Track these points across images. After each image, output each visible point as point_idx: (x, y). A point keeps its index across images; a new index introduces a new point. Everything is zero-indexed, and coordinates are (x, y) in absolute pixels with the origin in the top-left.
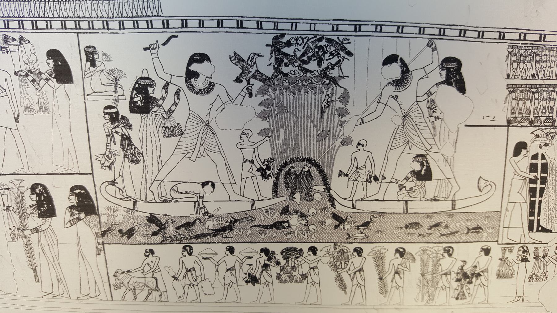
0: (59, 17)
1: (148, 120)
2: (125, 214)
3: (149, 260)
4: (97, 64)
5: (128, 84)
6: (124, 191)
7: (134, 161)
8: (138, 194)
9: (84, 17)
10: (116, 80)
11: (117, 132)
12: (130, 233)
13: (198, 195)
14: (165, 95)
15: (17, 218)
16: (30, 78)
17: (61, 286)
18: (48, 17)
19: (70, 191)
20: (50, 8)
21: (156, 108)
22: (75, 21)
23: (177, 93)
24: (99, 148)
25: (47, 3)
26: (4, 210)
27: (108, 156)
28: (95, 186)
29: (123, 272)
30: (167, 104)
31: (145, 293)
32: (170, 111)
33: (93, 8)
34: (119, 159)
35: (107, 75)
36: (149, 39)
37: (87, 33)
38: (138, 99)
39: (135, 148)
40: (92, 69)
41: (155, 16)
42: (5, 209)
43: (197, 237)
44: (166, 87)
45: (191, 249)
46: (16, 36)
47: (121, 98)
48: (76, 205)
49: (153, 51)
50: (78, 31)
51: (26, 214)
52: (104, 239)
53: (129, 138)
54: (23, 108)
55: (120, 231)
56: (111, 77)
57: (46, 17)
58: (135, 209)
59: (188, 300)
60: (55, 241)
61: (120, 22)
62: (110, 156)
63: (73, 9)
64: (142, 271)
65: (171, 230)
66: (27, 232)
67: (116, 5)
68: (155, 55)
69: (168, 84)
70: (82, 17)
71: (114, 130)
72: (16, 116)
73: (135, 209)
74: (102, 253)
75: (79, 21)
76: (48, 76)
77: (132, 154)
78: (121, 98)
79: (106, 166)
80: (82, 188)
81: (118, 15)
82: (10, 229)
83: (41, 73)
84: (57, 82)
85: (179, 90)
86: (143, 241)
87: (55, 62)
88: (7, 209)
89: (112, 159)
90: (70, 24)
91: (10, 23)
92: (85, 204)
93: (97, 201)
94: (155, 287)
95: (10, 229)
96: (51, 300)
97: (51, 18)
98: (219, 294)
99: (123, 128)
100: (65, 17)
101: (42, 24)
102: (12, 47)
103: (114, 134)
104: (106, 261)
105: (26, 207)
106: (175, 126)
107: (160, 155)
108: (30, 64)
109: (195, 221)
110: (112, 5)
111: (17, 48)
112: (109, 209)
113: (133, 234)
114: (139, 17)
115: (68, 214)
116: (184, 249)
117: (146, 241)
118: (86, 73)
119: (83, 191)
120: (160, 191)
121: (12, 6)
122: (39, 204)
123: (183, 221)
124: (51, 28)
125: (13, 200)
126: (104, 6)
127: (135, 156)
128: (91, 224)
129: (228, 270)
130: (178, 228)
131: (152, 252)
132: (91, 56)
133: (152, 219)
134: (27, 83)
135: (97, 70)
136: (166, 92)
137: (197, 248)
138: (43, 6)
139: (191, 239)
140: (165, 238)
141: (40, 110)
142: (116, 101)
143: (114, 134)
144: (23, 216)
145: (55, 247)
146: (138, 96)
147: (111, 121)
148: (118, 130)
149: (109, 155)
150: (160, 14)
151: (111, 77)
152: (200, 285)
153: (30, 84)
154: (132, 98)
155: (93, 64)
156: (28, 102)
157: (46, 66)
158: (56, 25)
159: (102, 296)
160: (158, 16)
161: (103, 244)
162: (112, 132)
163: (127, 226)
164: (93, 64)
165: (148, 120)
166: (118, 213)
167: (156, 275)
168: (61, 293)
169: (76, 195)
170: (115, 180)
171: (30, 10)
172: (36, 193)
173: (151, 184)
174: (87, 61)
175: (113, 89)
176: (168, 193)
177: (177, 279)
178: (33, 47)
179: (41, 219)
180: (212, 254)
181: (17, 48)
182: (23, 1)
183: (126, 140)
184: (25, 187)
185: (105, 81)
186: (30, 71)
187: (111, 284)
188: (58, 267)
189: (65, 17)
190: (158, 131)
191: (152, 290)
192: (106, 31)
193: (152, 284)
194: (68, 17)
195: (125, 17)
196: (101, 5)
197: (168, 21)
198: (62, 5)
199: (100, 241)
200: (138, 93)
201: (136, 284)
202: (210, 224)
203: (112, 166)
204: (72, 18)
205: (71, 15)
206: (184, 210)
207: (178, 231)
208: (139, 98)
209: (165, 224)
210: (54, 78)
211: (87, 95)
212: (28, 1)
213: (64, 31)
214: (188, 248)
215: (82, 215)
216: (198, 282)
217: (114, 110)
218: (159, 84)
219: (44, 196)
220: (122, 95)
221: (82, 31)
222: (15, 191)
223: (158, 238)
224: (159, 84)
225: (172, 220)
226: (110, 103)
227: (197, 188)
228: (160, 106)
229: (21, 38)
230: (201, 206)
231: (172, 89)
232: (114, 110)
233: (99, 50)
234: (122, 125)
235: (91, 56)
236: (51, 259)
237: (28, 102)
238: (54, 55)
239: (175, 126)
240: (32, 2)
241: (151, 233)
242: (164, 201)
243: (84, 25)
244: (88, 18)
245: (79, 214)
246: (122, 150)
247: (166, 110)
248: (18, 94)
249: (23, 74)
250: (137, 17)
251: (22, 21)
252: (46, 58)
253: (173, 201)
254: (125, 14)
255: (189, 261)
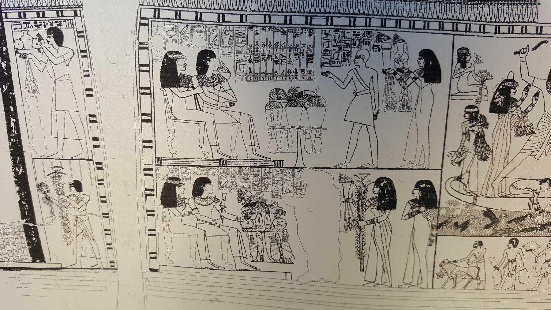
0: (438, 19)
1: (504, 120)
2: (463, 208)
3: (476, 252)
4: (468, 65)
5: (492, 85)
6: (468, 186)
7: (483, 158)
8: (480, 189)
9: (463, 20)
10: (483, 81)
11: (473, 131)
12: (465, 226)
13: (534, 192)
14: (524, 96)
15: (354, 209)
16: (398, 77)
17: (385, 275)
18: (427, 18)
19: (416, 186)
20: (430, 9)
21: (514, 108)
22: (453, 23)
23: (536, 95)
24: (453, 145)
25: (428, 4)
26: (343, 202)
27: (460, 153)
28: (441, 182)
29: (450, 262)
30: (524, 106)
31: (465, 282)
32: (526, 112)
33: (473, 12)
34: (470, 156)
35: (475, 76)
36: (520, 43)
37: (463, 35)
38: (500, 100)
39: (487, 146)
40: (462, 70)
41: (531, 22)
42: (344, 200)
43: (525, 231)
44: (527, 89)
45: (517, 241)
46: (391, 35)
47: (484, 98)
48: (418, 198)
49: (522, 55)
50: (455, 33)
51: (365, 206)
52: (439, 232)
53: (483, 137)
54: (384, 105)
55: (456, 224)
56: (478, 79)
57: (425, 18)
58: (474, 204)
59: (503, 288)
60: (389, 233)
61: (496, 26)
62: (462, 152)
63: (453, 11)
64: (467, 261)
65: (503, 224)
66: (362, 224)
67: (496, 10)
68: (524, 59)
69: (529, 86)
70: (461, 20)
71: (471, 129)
72: (375, 113)
73: (474, 204)
74: (434, 244)
75: (457, 23)
76: (417, 75)
77: (483, 152)
78: (484, 98)
79: (456, 163)
80: (428, 182)
81: (378, 13)
82: (345, 220)
83: (410, 72)
84: (425, 81)
85: (539, 92)
86: (475, 233)
87: (427, 62)
88: (347, 201)
89: (464, 155)
90: (448, 26)
91: (387, 22)
92: (427, 197)
93: (440, 195)
94: (475, 276)
95: (345, 220)
96: (371, 288)
97: (429, 18)
98: (533, 282)
99: (480, 127)
100: (444, 19)
101: (419, 24)
102: (385, 46)
103: (471, 133)
104: (436, 251)
105: (367, 199)
106: (528, 126)
107: (508, 154)
108: (400, 63)
109: (527, 215)
110: (491, 10)
111: (390, 46)
112: (450, 203)
113: (467, 227)
114: (516, 22)
115: (409, 207)
116: (511, 241)
117: (478, 233)
118: (455, 73)
119: (429, 186)
120: (500, 187)
121: (393, 6)
122: (381, 196)
123: (516, 216)
124: (428, 28)
125: (354, 192)
126: (483, 10)
127: (486, 154)
128: (429, 217)
129: (546, 261)
130: (509, 222)
131: (481, 243)
132: (463, 57)
133: (488, 213)
134: (393, 81)
135: (467, 71)
136: (526, 94)
137: (522, 241)
138: (423, 6)
139: (519, 232)
140: (496, 231)
141: (402, 107)
142: (479, 101)
143: (471, 133)
144: (361, 207)
145: (388, 239)
146: (499, 97)
147: (470, 120)
148: (475, 128)
149: (461, 152)
150: (536, 20)
151: (478, 79)
152: (517, 275)
153: (396, 82)
154: (494, 98)
155: (464, 66)
156: (391, 100)
157: (415, 64)
158: (434, 25)
159: (424, 285)
160: (534, 22)
161: (437, 235)
162: (469, 130)
163: (463, 219)
164: (464, 66)
165: (504, 120)
166: (458, 207)
167: (479, 265)
168: (384, 281)
169: (421, 189)
170: (461, 175)
171: (410, 10)
172: (380, 187)
173: (494, 180)
174: (458, 62)
175: (478, 89)
176: (508, 189)
177: (498, 269)
178: (407, 47)
179: (380, 211)
180: (535, 247)
181: (390, 46)
182: (404, 0)
183: (481, 137)
184: (369, 181)
185: (472, 81)
186: (399, 70)
187: (435, 272)
188: (387, 257)
189: (444, 19)
190: (511, 130)
191: (473, 278)
192: (482, 34)
193: (474, 274)
194: (447, 19)
195: (502, 22)
196: (481, 9)
197: (542, 27)
198: (443, 7)
199: (434, 233)
200: (501, 94)
201: (458, 273)
202: (540, 219)
203: (462, 162)
204: (451, 20)
205: (450, 17)
206: (519, 205)
207: (509, 225)
208: (500, 99)
209: (498, 219)
210: (422, 77)
211: (452, 95)
212: (410, 1)
213: (441, 32)
214: (514, 241)
215: (423, 209)
216: (517, 271)
217: (476, 110)
218: (522, 85)
219: (388, 190)
220: (486, 96)
221: (458, 33)
222: (359, 184)
223: (489, 231)
224: (522, 85)
225: (505, 214)
226: (472, 103)
227: (535, 185)
228: (518, 107)
229: (396, 37)
230: (535, 202)
231: (532, 91)
232: (476, 110)
233: (472, 52)
234: (480, 124)
235: (463, 57)
236: (381, 249)
237: (391, 100)
238: (427, 55)
239: (528, 126)
240: (413, 3)
241: (484, 225)
242: (503, 197)
243: (461, 27)
244: (466, 21)
245: (420, 207)
246: (474, 147)
247: (523, 111)
248: (382, 93)
249: (391, 72)
250: (513, 22)
251: (400, 20)
252: (418, 57)
253: (510, 196)
254: (502, 19)
255: (513, 253)
